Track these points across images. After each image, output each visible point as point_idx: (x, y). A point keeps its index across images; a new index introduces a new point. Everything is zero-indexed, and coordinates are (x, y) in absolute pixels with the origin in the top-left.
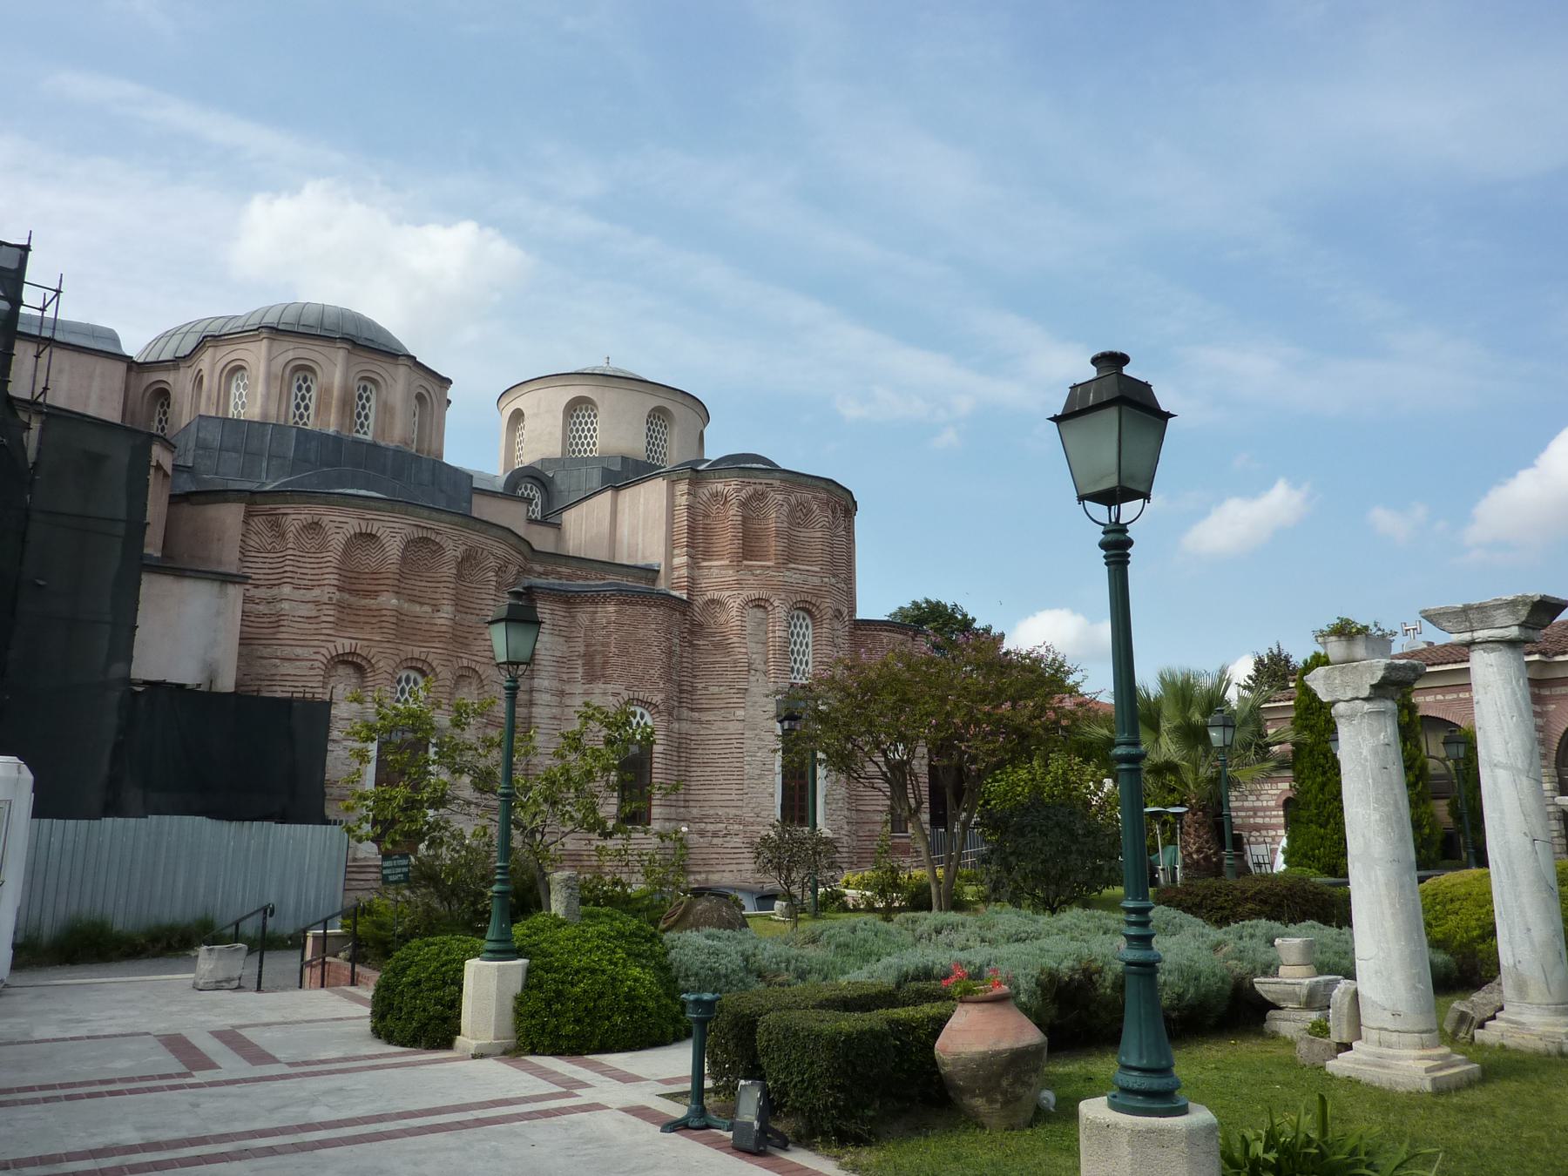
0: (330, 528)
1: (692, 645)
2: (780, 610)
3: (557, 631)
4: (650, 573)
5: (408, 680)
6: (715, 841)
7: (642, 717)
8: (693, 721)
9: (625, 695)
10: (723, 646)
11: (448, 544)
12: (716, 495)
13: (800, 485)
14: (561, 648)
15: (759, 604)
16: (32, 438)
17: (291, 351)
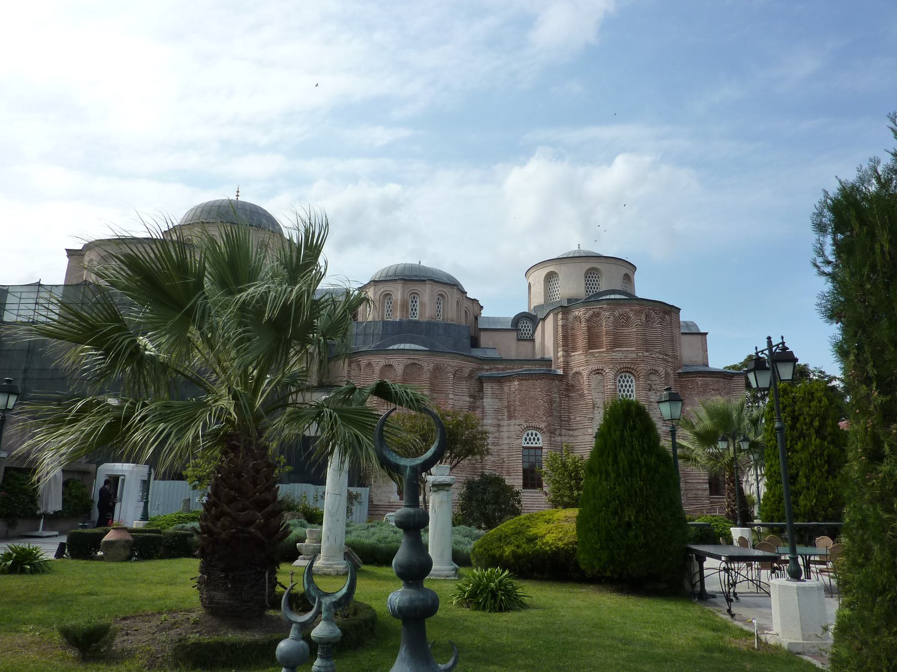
0: (374, 365)
1: (567, 396)
2: (610, 374)
3: (495, 396)
4: (548, 362)
5: (532, 434)
7: (536, 435)
8: (570, 436)
10: (582, 396)
12: (576, 318)
13: (621, 305)
14: (497, 404)
15: (598, 372)
17: (382, 288)
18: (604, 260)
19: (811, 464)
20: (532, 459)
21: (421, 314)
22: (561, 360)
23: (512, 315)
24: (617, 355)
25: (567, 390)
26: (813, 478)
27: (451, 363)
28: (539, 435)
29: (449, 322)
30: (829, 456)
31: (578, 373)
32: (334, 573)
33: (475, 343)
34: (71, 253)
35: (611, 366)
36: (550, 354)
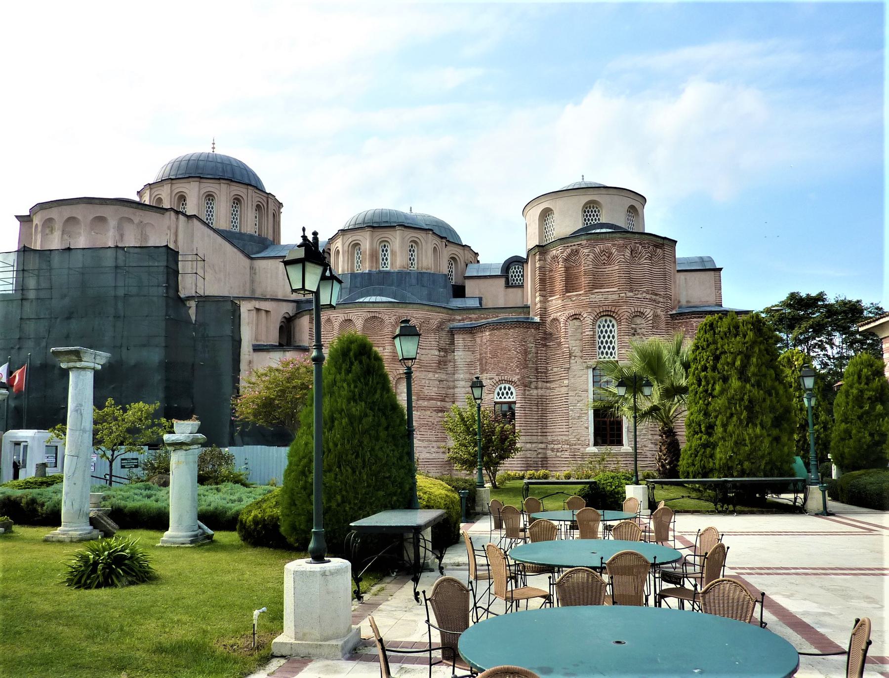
0: (333, 320)
1: (545, 345)
3: (467, 348)
5: (505, 388)
6: (559, 454)
7: (509, 389)
8: (547, 388)
9: (497, 378)
10: (560, 344)
11: (386, 318)
13: (602, 239)
14: (469, 357)
15: (576, 317)
16: (192, 312)
17: (350, 238)
18: (604, 191)
19: (729, 412)
21: (392, 264)
22: (538, 306)
24: (596, 297)
25: (545, 339)
26: (730, 428)
28: (513, 389)
29: (424, 271)
30: (750, 401)
31: (556, 320)
32: (67, 540)
33: (459, 292)
35: (589, 310)
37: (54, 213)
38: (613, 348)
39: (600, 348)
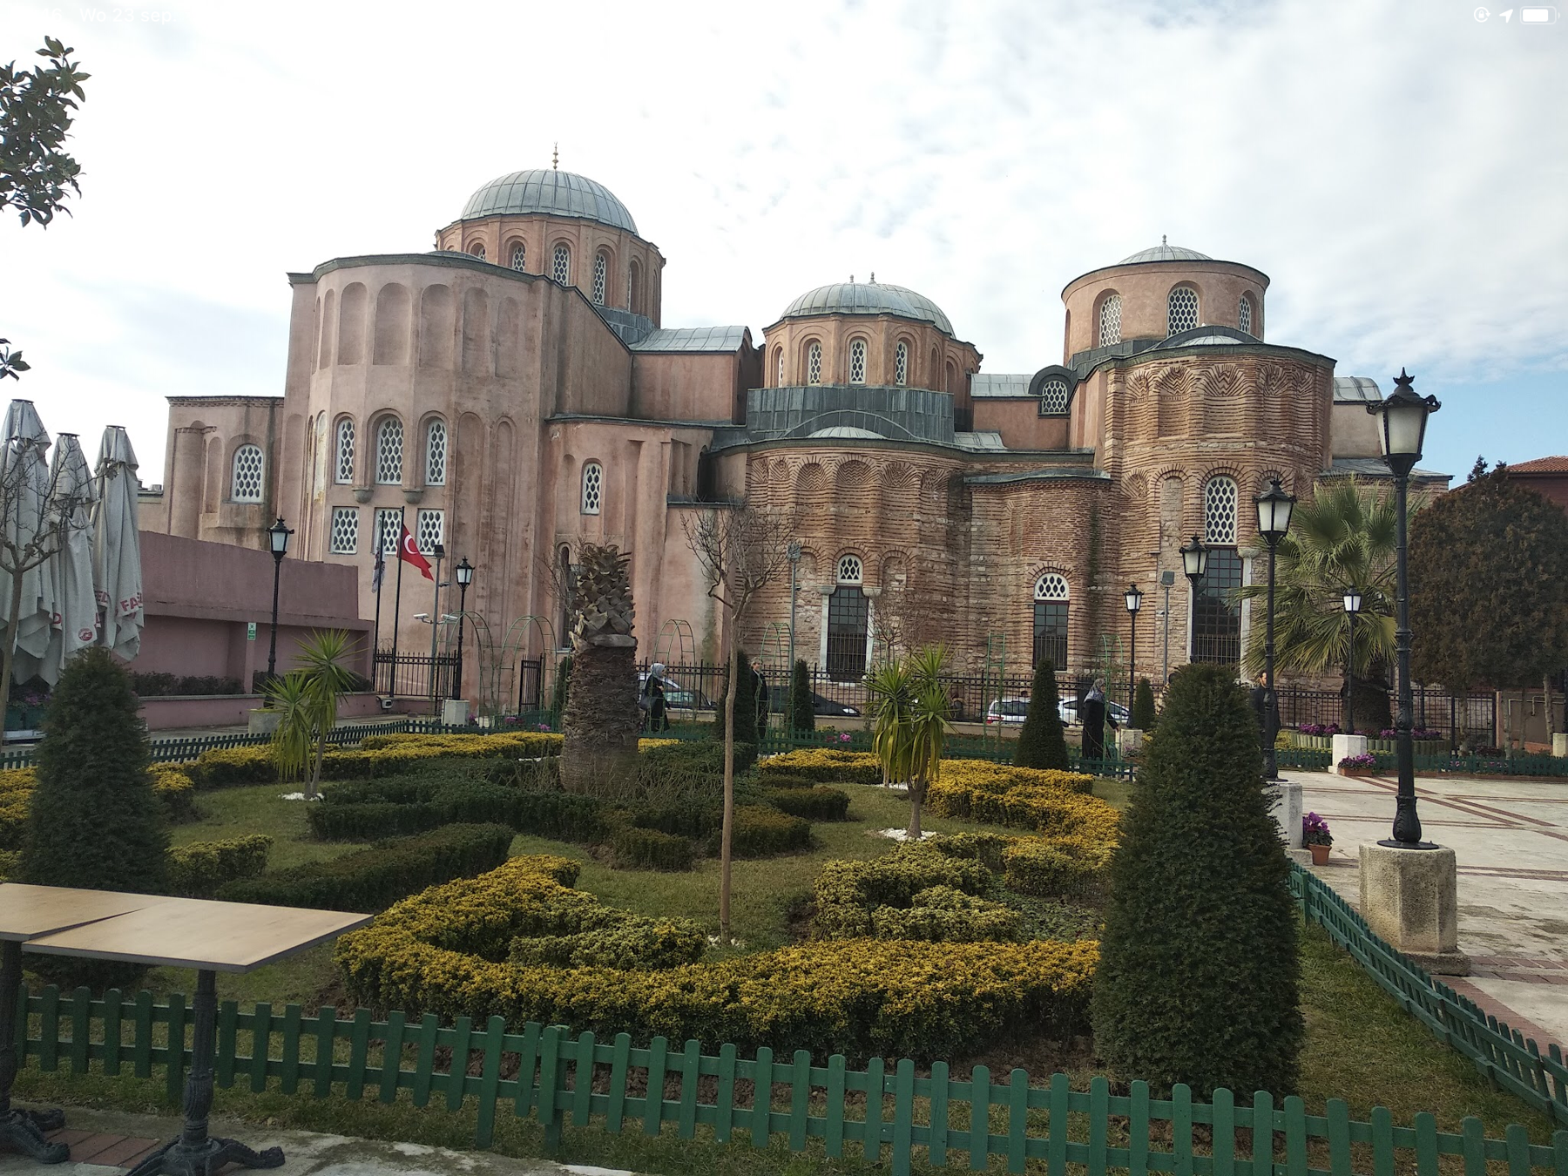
5: (1052, 580)
7: (1059, 581)
15: (1173, 475)
17: (805, 329)
20: (1051, 621)
23: (1032, 369)
27: (916, 461)
28: (1064, 582)
34: (296, 279)
36: (1089, 444)
37: (364, 276)
38: (1231, 526)
39: (1209, 524)
